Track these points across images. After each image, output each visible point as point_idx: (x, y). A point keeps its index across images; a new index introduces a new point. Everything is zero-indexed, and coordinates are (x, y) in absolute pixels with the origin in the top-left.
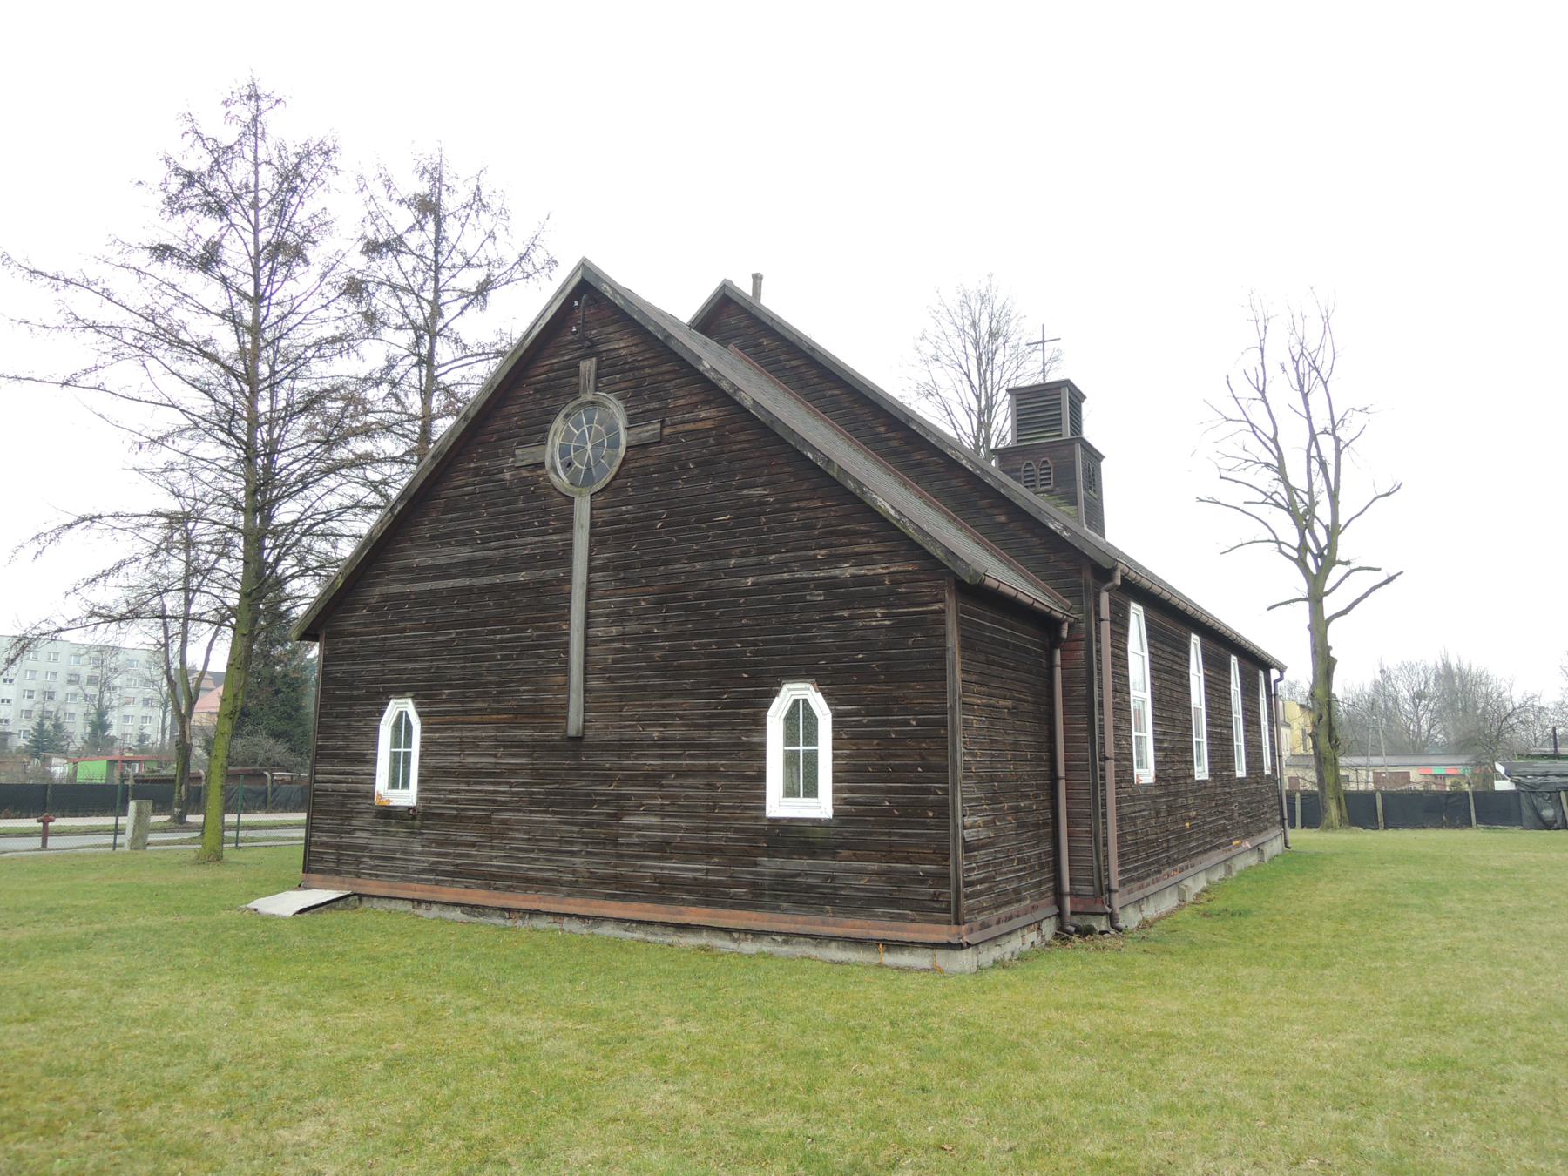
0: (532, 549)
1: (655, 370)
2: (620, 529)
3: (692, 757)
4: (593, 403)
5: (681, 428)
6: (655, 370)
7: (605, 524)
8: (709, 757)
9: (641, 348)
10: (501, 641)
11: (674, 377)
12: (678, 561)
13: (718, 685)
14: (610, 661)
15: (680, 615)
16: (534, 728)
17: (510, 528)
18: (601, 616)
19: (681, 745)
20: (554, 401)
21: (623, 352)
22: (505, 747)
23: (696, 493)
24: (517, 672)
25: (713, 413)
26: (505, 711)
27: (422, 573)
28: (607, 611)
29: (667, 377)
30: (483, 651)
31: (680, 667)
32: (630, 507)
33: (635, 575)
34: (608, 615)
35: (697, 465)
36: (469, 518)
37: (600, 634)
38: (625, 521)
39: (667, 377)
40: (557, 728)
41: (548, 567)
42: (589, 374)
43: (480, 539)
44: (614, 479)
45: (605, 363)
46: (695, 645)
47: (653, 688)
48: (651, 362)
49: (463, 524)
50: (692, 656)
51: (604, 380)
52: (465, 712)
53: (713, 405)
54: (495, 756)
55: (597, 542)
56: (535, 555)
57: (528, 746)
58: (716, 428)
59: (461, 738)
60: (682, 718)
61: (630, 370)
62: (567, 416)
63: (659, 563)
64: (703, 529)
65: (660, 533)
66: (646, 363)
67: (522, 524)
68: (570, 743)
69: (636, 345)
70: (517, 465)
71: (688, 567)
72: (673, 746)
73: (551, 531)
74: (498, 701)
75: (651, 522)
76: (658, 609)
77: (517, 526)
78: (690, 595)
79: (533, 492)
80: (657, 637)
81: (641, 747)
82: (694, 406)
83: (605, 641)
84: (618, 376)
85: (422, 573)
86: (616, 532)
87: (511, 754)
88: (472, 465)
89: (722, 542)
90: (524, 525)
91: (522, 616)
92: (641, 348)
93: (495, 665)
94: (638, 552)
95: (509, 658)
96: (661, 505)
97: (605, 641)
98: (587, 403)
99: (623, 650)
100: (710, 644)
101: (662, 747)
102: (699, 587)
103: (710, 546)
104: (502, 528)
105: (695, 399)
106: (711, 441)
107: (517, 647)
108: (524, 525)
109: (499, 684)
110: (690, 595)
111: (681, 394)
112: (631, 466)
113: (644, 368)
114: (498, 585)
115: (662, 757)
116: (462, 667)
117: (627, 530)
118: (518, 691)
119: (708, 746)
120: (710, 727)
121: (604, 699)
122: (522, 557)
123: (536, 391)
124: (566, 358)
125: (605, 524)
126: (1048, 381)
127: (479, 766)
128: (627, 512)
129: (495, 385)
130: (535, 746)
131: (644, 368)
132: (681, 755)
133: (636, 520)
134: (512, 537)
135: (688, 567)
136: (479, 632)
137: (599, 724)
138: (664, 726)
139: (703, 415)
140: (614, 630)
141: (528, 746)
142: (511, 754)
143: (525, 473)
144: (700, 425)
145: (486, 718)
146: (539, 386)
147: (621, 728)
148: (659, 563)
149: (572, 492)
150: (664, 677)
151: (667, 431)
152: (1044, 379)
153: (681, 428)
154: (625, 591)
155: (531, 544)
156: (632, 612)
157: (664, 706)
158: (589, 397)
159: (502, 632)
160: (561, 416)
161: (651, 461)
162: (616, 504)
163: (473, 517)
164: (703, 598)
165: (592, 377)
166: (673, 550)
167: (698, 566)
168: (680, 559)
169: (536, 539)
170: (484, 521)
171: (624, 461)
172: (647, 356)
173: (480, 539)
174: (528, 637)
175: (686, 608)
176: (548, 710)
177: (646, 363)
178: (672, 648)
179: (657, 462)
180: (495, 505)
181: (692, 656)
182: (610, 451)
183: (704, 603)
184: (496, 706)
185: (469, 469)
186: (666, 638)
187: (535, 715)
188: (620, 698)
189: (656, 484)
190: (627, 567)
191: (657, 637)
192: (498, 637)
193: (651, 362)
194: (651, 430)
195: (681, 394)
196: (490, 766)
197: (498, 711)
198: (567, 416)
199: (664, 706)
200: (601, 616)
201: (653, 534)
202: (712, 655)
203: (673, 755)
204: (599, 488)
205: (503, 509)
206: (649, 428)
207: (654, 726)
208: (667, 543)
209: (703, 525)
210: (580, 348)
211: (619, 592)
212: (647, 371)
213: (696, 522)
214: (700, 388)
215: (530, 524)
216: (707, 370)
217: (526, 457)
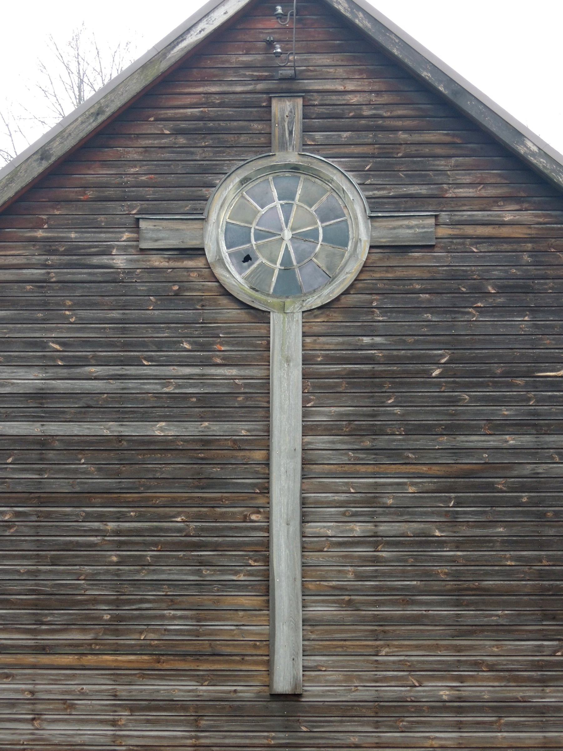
0: (179, 386)
1: (416, 137)
2: (362, 371)
3: (515, 727)
4: (295, 168)
5: (470, 230)
6: (416, 137)
7: (330, 360)
8: (543, 727)
9: (385, 99)
10: (118, 533)
11: (452, 152)
12: (472, 430)
13: (554, 619)
14: (350, 576)
15: (485, 512)
16: (201, 679)
17: (127, 346)
18: (331, 504)
19: (494, 709)
20: (216, 153)
21: (354, 99)
22: (132, 709)
23: (502, 331)
24: (156, 584)
25: (527, 216)
26: (130, 650)
27: (146, 286)
28: (342, 497)
29: (438, 150)
30: (78, 546)
31: (487, 591)
32: (378, 340)
33: (394, 445)
34: (340, 504)
35: (502, 290)
36: (36, 321)
37: (330, 533)
38: (370, 360)
39: (438, 150)
40: (247, 677)
41: (217, 418)
42: (291, 123)
43: (62, 358)
44: (346, 292)
45: (318, 110)
46: (512, 558)
47: (435, 621)
48: (408, 123)
49: (20, 330)
50: (508, 574)
51: (318, 136)
52: (42, 650)
53: (525, 205)
54: (114, 723)
55: (314, 386)
56: (186, 397)
57: (185, 708)
58: (531, 239)
59: (32, 692)
60: (492, 668)
61: (368, 129)
62: (245, 181)
63: (439, 430)
64: (518, 385)
65: (439, 385)
66: (399, 123)
67: (155, 343)
68: (274, 705)
69: (378, 93)
70: (144, 245)
71: (493, 441)
72: (480, 710)
73: (219, 361)
74: (116, 632)
75: (427, 367)
76: (441, 500)
77: (144, 344)
78: (500, 483)
79: (177, 294)
80: (441, 544)
81: (419, 710)
82: (496, 199)
83: (340, 544)
84: (345, 134)
85: (146, 286)
86: (352, 374)
87: (148, 721)
88: (40, 234)
89: (554, 409)
90: (160, 346)
91: (163, 495)
92: (385, 99)
93: (107, 572)
94: (397, 410)
95: (139, 562)
96: (440, 343)
97: (340, 544)
98: (286, 166)
99: (376, 560)
100: (539, 559)
101: (460, 710)
102: (515, 473)
103: (530, 414)
104: (111, 345)
105: (491, 192)
106: (526, 258)
107: (155, 544)
108: (160, 346)
109: (117, 603)
110: (500, 483)
111: (468, 180)
112: (377, 275)
113: (395, 130)
114: (105, 439)
115: (459, 726)
116: (28, 572)
117: (374, 375)
118: (163, 617)
119: (542, 711)
120: (544, 682)
121: (344, 636)
122: (158, 396)
123: (178, 132)
124: (239, 89)
125: (330, 360)
126: (97, 91)
127: (78, 740)
128: (372, 346)
129: (109, 111)
130: (203, 708)
131: (395, 130)
132: (491, 723)
133: (391, 360)
134: (136, 362)
135: (493, 441)
136: (66, 514)
137: (333, 676)
138: (461, 679)
139: (508, 217)
140: (358, 529)
141: (185, 708)
142: (148, 721)
143: (157, 261)
144: (505, 231)
145: (90, 660)
146: (183, 125)
147: (376, 681)
148: (439, 430)
149: (266, 304)
150: (458, 604)
151: (443, 231)
152: (94, 90)
153: (470, 230)
154: (376, 469)
155: (175, 378)
156: (390, 502)
157: (458, 649)
158: (293, 158)
159: (119, 517)
160: (236, 179)
161: (416, 273)
162: (352, 331)
163: (44, 321)
164: (523, 488)
165: (297, 128)
166: (464, 413)
167: (512, 441)
168: (479, 427)
169: (187, 371)
170: (69, 330)
171: (365, 267)
172: (400, 112)
173: (62, 358)
174: (180, 530)
175: (493, 503)
176: (228, 650)
177: (399, 123)
178: (469, 562)
179: (426, 275)
180: (92, 305)
181: (508, 574)
182: (329, 248)
183: (525, 497)
184: (110, 639)
185: (33, 240)
186: (458, 546)
187: (198, 656)
188: (375, 635)
189: (428, 309)
190: (376, 432)
191: (441, 544)
192: (111, 526)
193: (408, 123)
194: (418, 226)
195: (468, 180)
196: (103, 740)
197: (116, 650)
198: (245, 181)
199: (458, 649)
200: (331, 504)
201: (424, 384)
202: (541, 575)
203: (478, 723)
204: (319, 303)
205: (115, 314)
206: (413, 222)
207: (442, 678)
208: (453, 401)
209: (519, 381)
210: (265, 79)
211: (362, 469)
212: (402, 136)
213: (506, 374)
214: (499, 175)
215: (174, 345)
216: (533, 154)
217: (161, 235)
